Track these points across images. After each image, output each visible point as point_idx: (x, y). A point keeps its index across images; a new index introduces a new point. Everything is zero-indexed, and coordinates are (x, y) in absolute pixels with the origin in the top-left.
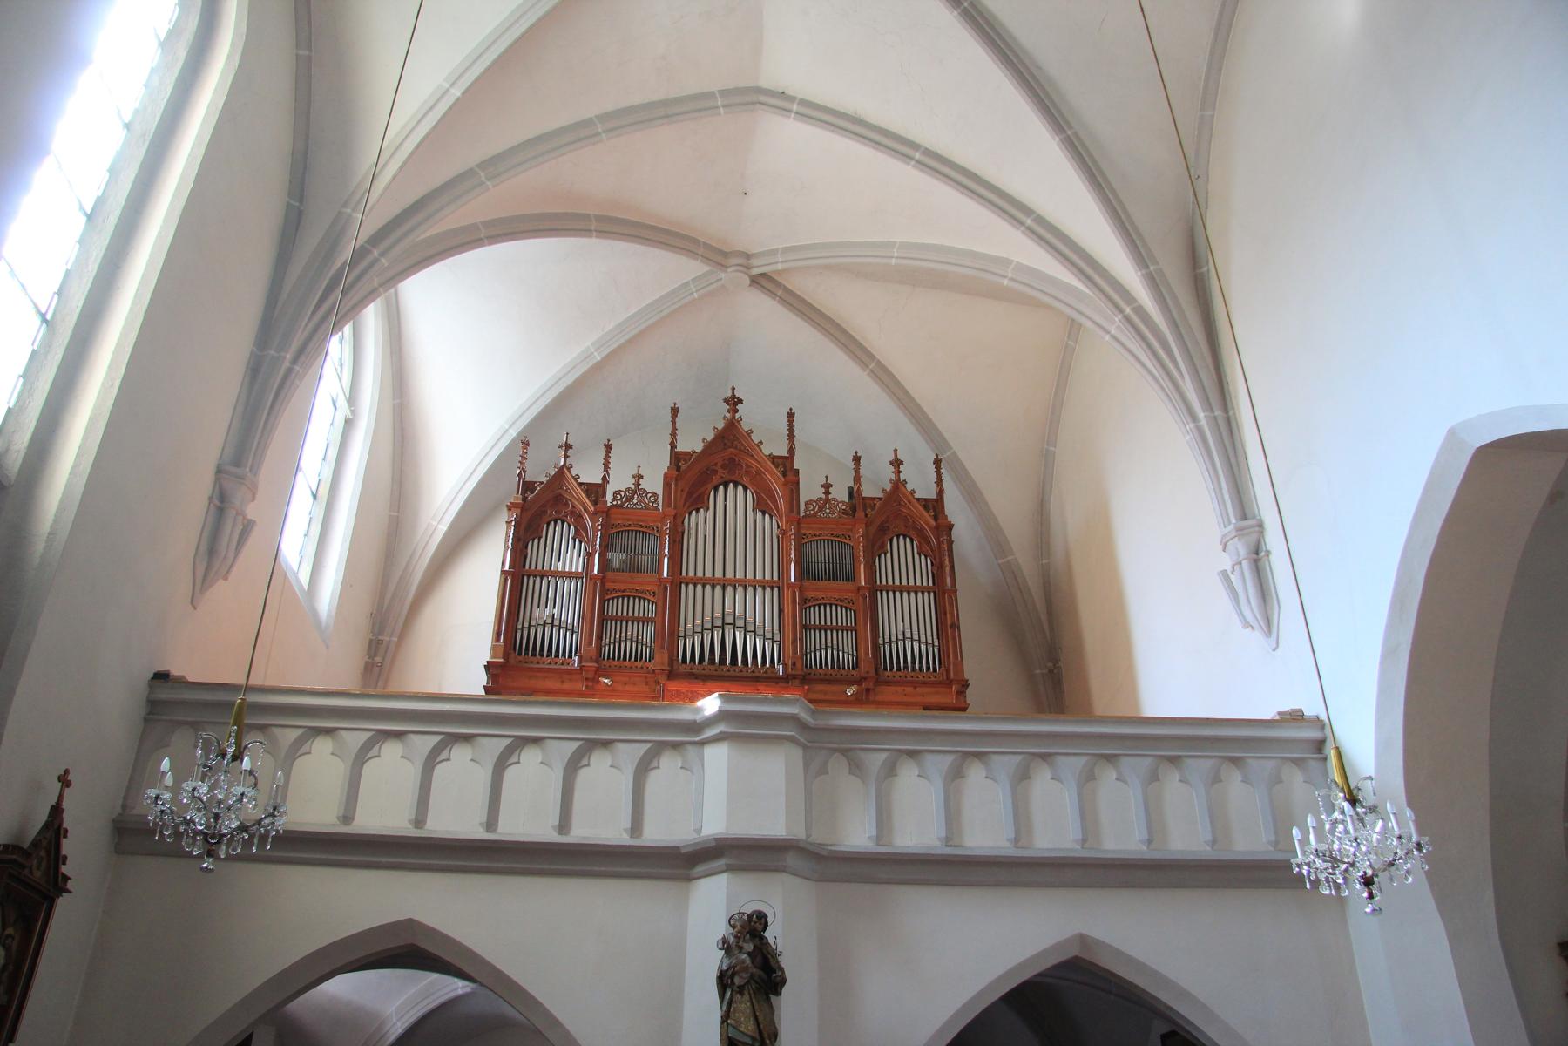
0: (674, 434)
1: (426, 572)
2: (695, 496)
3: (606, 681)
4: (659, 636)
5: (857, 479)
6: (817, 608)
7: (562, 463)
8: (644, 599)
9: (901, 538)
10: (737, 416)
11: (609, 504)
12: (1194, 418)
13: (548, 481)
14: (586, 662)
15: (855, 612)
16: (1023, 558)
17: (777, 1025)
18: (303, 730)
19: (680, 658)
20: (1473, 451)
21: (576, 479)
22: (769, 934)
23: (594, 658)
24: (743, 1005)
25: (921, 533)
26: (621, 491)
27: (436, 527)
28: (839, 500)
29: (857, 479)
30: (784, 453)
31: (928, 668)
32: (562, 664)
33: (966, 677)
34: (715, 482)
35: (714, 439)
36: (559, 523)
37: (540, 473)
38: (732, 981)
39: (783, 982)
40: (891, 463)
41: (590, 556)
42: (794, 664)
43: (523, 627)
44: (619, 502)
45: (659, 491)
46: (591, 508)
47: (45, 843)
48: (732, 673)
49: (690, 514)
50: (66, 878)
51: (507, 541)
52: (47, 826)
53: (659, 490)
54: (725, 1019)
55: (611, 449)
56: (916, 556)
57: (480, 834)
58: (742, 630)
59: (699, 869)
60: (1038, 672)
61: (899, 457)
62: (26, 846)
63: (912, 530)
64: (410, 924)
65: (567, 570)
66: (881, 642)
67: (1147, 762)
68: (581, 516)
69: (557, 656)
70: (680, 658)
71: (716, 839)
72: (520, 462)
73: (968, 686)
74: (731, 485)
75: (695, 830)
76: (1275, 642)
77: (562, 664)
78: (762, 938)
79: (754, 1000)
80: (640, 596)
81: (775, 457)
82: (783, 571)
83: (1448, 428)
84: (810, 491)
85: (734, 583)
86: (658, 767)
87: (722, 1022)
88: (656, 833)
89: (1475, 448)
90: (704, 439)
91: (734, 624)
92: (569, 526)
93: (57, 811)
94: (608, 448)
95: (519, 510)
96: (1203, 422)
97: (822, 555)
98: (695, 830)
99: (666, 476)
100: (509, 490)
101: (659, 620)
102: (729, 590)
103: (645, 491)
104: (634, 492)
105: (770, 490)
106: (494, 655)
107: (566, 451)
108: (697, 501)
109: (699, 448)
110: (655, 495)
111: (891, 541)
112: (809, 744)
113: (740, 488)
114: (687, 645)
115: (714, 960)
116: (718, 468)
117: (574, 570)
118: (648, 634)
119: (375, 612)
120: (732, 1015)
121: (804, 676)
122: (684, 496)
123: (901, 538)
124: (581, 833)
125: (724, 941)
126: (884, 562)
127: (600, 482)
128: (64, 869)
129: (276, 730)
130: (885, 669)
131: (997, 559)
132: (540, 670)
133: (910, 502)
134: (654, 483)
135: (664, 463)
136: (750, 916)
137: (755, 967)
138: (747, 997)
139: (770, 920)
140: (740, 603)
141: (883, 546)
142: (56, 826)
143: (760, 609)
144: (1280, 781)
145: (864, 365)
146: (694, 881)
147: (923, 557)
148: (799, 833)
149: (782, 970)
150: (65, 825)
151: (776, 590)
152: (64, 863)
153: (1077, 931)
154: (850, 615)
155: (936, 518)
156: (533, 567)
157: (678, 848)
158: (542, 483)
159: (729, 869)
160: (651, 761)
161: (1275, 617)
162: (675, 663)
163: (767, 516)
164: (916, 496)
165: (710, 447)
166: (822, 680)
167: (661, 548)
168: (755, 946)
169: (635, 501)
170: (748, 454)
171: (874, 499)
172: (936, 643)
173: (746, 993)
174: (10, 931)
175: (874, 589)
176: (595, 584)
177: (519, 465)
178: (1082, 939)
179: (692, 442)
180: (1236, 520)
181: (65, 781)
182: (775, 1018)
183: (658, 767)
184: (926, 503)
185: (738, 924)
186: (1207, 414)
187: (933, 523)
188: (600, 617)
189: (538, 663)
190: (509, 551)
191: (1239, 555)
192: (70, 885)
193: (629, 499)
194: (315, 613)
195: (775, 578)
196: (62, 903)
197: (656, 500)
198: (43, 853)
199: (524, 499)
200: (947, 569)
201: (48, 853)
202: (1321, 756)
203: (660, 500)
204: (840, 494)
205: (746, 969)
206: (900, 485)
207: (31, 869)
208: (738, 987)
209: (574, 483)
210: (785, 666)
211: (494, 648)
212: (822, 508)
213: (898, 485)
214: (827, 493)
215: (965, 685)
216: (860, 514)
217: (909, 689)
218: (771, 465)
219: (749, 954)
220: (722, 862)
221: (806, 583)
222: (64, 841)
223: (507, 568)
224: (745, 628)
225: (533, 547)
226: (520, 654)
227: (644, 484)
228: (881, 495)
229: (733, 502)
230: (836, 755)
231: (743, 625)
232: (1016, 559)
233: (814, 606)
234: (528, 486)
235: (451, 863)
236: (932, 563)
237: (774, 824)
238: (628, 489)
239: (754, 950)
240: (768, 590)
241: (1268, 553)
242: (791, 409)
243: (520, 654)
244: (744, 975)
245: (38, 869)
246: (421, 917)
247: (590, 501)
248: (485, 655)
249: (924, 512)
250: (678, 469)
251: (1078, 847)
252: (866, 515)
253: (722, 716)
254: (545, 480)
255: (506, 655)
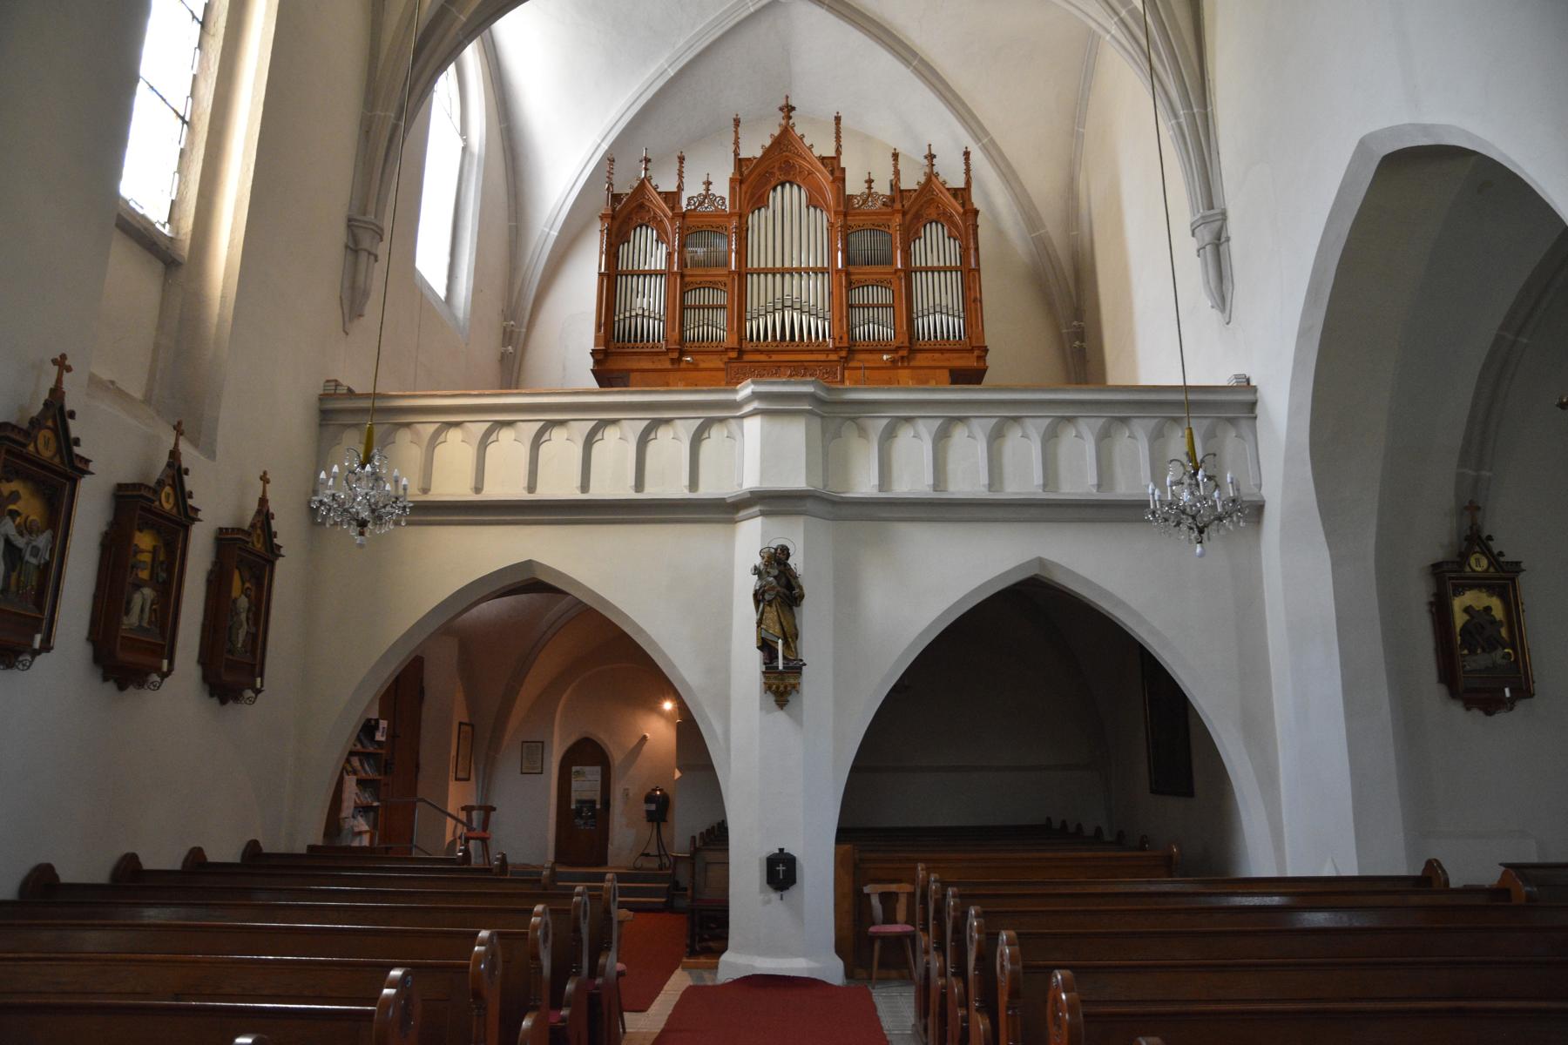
0: (736, 143)
1: (545, 269)
2: (757, 196)
3: (689, 359)
4: (730, 320)
5: (897, 173)
6: (865, 288)
7: (643, 176)
8: (717, 289)
9: (934, 224)
10: (791, 122)
11: (684, 210)
12: (1176, 116)
13: (632, 193)
14: (672, 345)
15: (893, 291)
16: (1052, 227)
17: (798, 627)
18: (439, 424)
19: (748, 337)
20: (1380, 159)
21: (655, 189)
22: (791, 561)
23: (677, 341)
24: (771, 614)
25: (950, 219)
26: (694, 197)
27: (548, 233)
28: (880, 193)
29: (897, 173)
30: (832, 153)
31: (955, 336)
32: (652, 347)
33: (987, 344)
34: (773, 183)
35: (762, 157)
36: (644, 228)
37: (625, 187)
38: (763, 596)
39: (802, 597)
40: (926, 157)
41: (669, 255)
42: (841, 338)
43: (625, 317)
44: (693, 207)
45: (727, 196)
46: (670, 214)
47: (259, 525)
48: (790, 348)
49: (753, 213)
50: (279, 547)
51: (601, 248)
52: (259, 512)
53: (726, 194)
54: (759, 623)
55: (684, 159)
56: (947, 240)
57: (577, 495)
58: (799, 311)
59: (742, 514)
60: (1064, 331)
61: (933, 152)
62: (246, 527)
63: (944, 218)
64: (529, 564)
65: (653, 268)
66: (915, 316)
67: (1101, 422)
68: (661, 221)
69: (648, 341)
70: (748, 337)
71: (751, 492)
72: (608, 177)
73: (988, 350)
74: (788, 185)
75: (738, 485)
76: (1228, 316)
77: (652, 347)
78: (786, 565)
79: (779, 611)
80: (713, 286)
81: (824, 158)
82: (833, 259)
83: (1359, 138)
84: (854, 186)
85: (791, 271)
86: (709, 437)
87: (758, 627)
88: (709, 488)
89: (532, 576)
90: (763, 146)
91: (792, 307)
92: (653, 230)
93: (263, 501)
94: (681, 159)
95: (609, 220)
96: (1182, 120)
97: (864, 243)
98: (738, 485)
99: (732, 180)
100: (601, 203)
101: (729, 306)
102: (787, 277)
103: (714, 195)
104: (705, 197)
105: (821, 188)
106: (596, 344)
107: (646, 165)
108: (759, 202)
109: (758, 153)
110: (723, 198)
111: (925, 227)
112: (826, 415)
113: (795, 188)
114: (754, 326)
115: (752, 582)
116: (776, 170)
117: (658, 268)
118: (721, 318)
119: (505, 309)
120: (764, 622)
121: (849, 348)
122: (748, 197)
123: (934, 224)
124: (652, 491)
125: (756, 568)
126: (918, 246)
127: (675, 190)
128: (276, 541)
129: (418, 426)
130: (919, 339)
131: (1030, 234)
132: (635, 354)
133: (941, 192)
134: (722, 189)
135: (729, 170)
136: (776, 550)
137: (781, 586)
138: (774, 608)
139: (791, 552)
140: (795, 287)
141: (918, 231)
142: (265, 511)
143: (814, 291)
144: (1216, 436)
145: (907, 63)
146: (738, 524)
147: (952, 240)
148: (817, 485)
149: (800, 588)
150: (271, 510)
151: (826, 275)
152: (275, 537)
153: (1038, 555)
154: (889, 293)
155: (963, 205)
156: (625, 268)
157: (724, 499)
158: (627, 194)
159: (763, 514)
160: (703, 433)
161: (1230, 295)
162: (744, 341)
163: (818, 210)
164: (947, 186)
165: (768, 152)
166: (863, 350)
167: (730, 245)
168: (780, 571)
169: (706, 205)
170: (800, 156)
171: (910, 191)
172: (962, 315)
173: (774, 605)
174: (247, 585)
175: (909, 272)
176: (676, 279)
177: (607, 179)
178: (1041, 561)
179: (753, 149)
180: (1204, 209)
181: (265, 479)
182: (797, 621)
183: (709, 437)
184: (955, 192)
185: (766, 556)
186: (1186, 111)
187: (961, 210)
188: (680, 308)
189: (633, 348)
190: (604, 256)
191: (1203, 240)
192: (283, 551)
193: (701, 204)
194: (455, 318)
195: (826, 265)
196: (279, 563)
197: (724, 203)
198: (259, 531)
199: (613, 210)
200: (972, 252)
201: (263, 531)
202: (1251, 415)
203: (727, 202)
204: (882, 188)
205: (773, 588)
206: (933, 178)
207: (253, 543)
208: (768, 601)
209: (655, 193)
210: (834, 339)
211: (597, 338)
212: (865, 201)
213: (931, 176)
214: (870, 188)
215: (986, 350)
216: (898, 206)
217: (937, 355)
218: (821, 165)
219: (775, 577)
220: (756, 509)
221: (851, 269)
222: (273, 522)
223: (603, 270)
224: (801, 309)
225: (623, 250)
226: (618, 341)
227: (713, 190)
228: (917, 187)
229: (789, 198)
230: (848, 422)
231: (799, 307)
232: (1047, 232)
233: (859, 288)
234: (616, 198)
235: (560, 517)
236: (960, 247)
237: (797, 481)
238: (700, 195)
239: (779, 575)
240: (820, 275)
241: (1228, 239)
242: (838, 113)
243: (618, 341)
244: (772, 592)
245: (258, 542)
246: (534, 559)
247: (669, 207)
248: (591, 345)
249: (952, 200)
250: (741, 174)
251: (1041, 491)
252: (903, 206)
253: (756, 396)
254: (630, 191)
255: (607, 343)
